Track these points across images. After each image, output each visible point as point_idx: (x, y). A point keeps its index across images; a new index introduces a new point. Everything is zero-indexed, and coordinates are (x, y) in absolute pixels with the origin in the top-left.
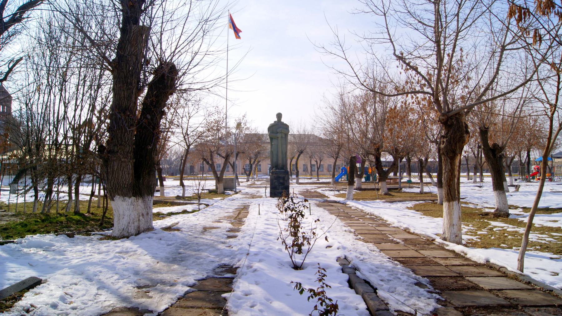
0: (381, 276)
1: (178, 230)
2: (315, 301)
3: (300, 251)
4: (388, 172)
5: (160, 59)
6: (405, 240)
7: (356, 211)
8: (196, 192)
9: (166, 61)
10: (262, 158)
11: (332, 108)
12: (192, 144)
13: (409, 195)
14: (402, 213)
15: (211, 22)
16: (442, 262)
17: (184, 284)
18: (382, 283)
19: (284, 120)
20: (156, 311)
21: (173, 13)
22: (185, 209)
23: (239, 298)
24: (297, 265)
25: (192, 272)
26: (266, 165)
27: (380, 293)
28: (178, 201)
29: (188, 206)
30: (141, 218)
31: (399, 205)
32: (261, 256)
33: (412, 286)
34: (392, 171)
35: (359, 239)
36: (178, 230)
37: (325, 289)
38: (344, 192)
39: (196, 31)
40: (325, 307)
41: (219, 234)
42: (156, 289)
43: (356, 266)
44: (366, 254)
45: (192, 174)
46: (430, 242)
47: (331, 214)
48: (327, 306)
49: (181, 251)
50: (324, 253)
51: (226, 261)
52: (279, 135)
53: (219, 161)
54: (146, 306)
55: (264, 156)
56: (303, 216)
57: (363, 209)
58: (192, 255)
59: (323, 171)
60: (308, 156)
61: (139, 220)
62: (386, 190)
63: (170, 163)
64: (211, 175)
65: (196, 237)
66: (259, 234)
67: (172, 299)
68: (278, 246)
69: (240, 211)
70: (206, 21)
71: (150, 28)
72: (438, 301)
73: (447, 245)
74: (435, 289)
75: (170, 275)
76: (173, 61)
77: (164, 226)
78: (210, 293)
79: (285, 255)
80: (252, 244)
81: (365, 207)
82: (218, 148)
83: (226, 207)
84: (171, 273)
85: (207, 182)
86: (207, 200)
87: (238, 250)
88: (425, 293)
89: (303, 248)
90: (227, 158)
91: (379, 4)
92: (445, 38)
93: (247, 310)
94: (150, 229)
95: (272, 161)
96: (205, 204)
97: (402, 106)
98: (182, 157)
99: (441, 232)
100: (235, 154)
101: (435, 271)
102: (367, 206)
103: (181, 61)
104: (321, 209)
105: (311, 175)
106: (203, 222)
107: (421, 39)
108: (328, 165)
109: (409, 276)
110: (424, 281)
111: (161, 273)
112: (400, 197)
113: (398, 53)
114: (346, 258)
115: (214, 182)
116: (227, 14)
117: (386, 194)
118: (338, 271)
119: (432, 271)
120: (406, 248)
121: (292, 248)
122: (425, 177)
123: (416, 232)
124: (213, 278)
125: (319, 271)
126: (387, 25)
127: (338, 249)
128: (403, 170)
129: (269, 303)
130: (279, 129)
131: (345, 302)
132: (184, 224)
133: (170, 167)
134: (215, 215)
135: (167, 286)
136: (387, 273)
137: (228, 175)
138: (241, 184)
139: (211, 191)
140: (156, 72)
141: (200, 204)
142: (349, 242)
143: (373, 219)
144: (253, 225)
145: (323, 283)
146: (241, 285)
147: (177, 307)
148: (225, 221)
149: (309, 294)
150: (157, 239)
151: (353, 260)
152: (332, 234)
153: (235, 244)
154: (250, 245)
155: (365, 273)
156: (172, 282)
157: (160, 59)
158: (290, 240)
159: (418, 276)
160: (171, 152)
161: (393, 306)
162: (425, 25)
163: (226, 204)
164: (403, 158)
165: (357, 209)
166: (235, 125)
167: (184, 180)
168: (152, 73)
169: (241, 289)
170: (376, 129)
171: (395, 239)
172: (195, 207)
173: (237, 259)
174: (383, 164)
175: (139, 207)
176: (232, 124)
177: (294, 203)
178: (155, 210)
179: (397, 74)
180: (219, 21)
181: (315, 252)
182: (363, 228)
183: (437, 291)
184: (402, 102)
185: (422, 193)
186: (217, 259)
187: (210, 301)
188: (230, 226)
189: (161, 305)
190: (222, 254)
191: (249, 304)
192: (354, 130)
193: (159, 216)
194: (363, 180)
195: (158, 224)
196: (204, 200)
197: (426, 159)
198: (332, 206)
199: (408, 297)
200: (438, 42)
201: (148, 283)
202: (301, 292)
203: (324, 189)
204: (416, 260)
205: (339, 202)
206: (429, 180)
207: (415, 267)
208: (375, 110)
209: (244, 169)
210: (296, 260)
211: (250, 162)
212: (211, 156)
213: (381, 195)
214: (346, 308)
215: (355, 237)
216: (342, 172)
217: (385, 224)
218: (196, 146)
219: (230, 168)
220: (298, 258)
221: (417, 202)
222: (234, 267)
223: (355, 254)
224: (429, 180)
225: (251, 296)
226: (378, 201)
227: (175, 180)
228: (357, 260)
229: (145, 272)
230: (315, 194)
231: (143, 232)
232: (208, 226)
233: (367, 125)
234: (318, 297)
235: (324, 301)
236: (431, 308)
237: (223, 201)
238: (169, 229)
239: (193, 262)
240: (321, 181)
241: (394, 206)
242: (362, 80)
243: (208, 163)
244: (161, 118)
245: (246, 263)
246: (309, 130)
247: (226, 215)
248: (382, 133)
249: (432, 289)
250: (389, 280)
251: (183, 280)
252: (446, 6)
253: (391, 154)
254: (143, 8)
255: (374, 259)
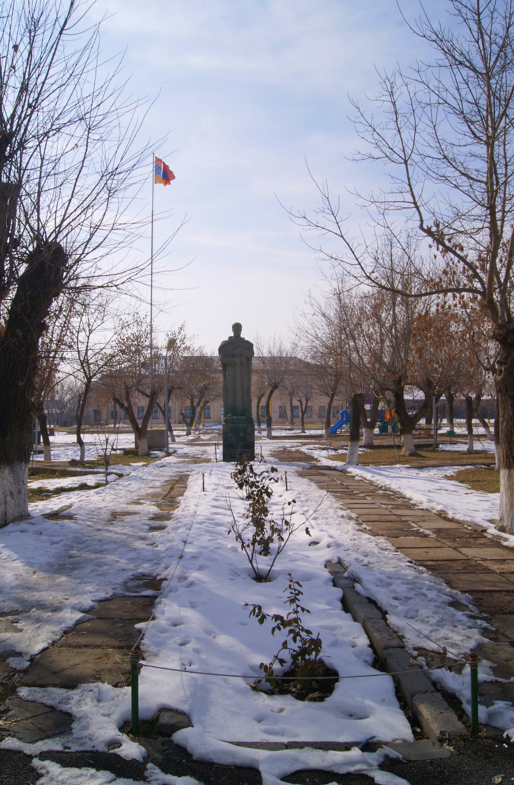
0: (395, 592)
1: (70, 517)
2: (283, 634)
3: (266, 551)
4: (417, 418)
5: (37, 237)
6: (438, 531)
7: (362, 483)
8: (102, 453)
9: (47, 240)
10: (212, 397)
11: (324, 315)
12: (95, 375)
13: (450, 456)
14: (437, 486)
15: (121, 176)
16: (495, 567)
17: (74, 608)
18: (396, 603)
19: (245, 335)
20: (27, 654)
21: (57, 161)
22: (85, 482)
23: (163, 631)
24: (261, 573)
25: (89, 588)
26: (217, 408)
27: (392, 619)
28: (74, 469)
29: (89, 477)
30: (9, 499)
31: (433, 472)
32: (202, 561)
33: (443, 608)
34: (423, 416)
35: (364, 531)
36: (70, 517)
37: (301, 615)
38: (344, 451)
39: (96, 191)
40: (300, 644)
41: (136, 524)
42: (29, 617)
43: (355, 575)
44: (373, 554)
45: (98, 424)
46: (477, 534)
47: (321, 488)
48: (304, 641)
49: (73, 552)
50: (306, 553)
51: (145, 568)
52: (237, 360)
53: (141, 402)
54: (11, 645)
55: (214, 393)
56: (269, 495)
57: (374, 479)
58: (91, 560)
59: (311, 417)
60: (287, 392)
61: (6, 502)
62: (412, 447)
63: (61, 404)
64: (128, 426)
65: (99, 530)
66: (202, 523)
67: (54, 632)
68: (231, 543)
69: (174, 485)
70: (112, 173)
71: (19, 185)
72: (484, 632)
73: (506, 540)
74: (481, 612)
75: (53, 593)
76: (58, 241)
77: (48, 512)
78: (117, 622)
79: (241, 558)
80: (189, 540)
81: (377, 477)
82: (139, 382)
83: (150, 478)
84: (55, 590)
85: (121, 436)
86: (120, 466)
87: (166, 550)
88: (465, 619)
89: (271, 545)
90: (153, 397)
91: (395, 144)
92: (504, 200)
93: (174, 650)
94: (25, 516)
95: (226, 402)
96: (116, 474)
97: (437, 310)
98: (80, 396)
99: (497, 517)
100: (165, 391)
101: (483, 582)
102: (380, 474)
103: (72, 240)
104: (305, 481)
105: (292, 423)
106: (111, 504)
107: (465, 204)
108: (320, 407)
109: (440, 591)
110: (464, 598)
111: (38, 590)
112: (435, 459)
113: (428, 223)
114: (340, 562)
115: (132, 437)
116: (150, 160)
117: (412, 455)
118: (326, 583)
119: (478, 582)
120: (439, 544)
121: (251, 546)
122: (477, 425)
123: (457, 517)
124: (123, 596)
125: (290, 586)
126: (409, 179)
127: (329, 546)
128: (441, 413)
129: (211, 638)
130: (236, 348)
131: (335, 635)
132: (80, 508)
133: (62, 413)
134: (132, 492)
135: (47, 612)
136: (405, 587)
137: (156, 426)
138: (177, 439)
139: (127, 452)
140: (31, 258)
141: (108, 474)
142: (346, 536)
143: (387, 497)
144: (192, 508)
145: (298, 606)
146: (167, 609)
147: (62, 646)
148: (148, 503)
149: (275, 624)
150: (35, 533)
151: (351, 564)
152: (320, 521)
153: (161, 540)
154: (185, 542)
155: (369, 586)
156: (56, 604)
157: (37, 237)
158: (249, 534)
159: (455, 591)
160: (63, 387)
161: (412, 640)
162: (472, 179)
163: (150, 474)
164: (441, 395)
165: (363, 480)
166: (165, 343)
167: (84, 433)
168: (24, 261)
169: (167, 615)
170: (395, 348)
171: (422, 530)
172: (101, 478)
173: (163, 565)
174: (407, 405)
175: (5, 481)
176: (161, 341)
177: (256, 475)
178: (35, 485)
179: (429, 259)
180: (134, 173)
181: (290, 553)
182: (372, 511)
183: (484, 615)
184: (438, 305)
185: (470, 452)
186: (131, 566)
187: (116, 636)
188: (154, 509)
189: (37, 643)
190: (139, 558)
191: (178, 640)
192: (361, 351)
193: (43, 494)
194: (376, 431)
195: (37, 507)
196: (115, 466)
197: (478, 397)
198: (324, 475)
199: (437, 625)
200: (492, 208)
201: (17, 606)
202: (261, 621)
203: (312, 446)
204: (454, 564)
205: (334, 469)
206: (481, 430)
207: (451, 577)
208: (394, 316)
209: (182, 414)
210: (260, 566)
211: (192, 402)
212: (128, 395)
213: (404, 456)
214: (335, 644)
215: (357, 527)
216: (342, 418)
217: (407, 504)
218: (103, 377)
219: (160, 414)
220: (262, 563)
221: (462, 468)
222: (158, 578)
223: (355, 555)
224: (481, 430)
225: (182, 626)
226: (398, 466)
227: (69, 433)
228: (359, 566)
229: (12, 588)
230: (297, 455)
231: (13, 521)
232: (119, 510)
233: (382, 341)
234: (288, 628)
235: (298, 634)
236: (472, 644)
237: (146, 469)
238: (55, 515)
239: (92, 571)
240: (308, 433)
241: (423, 474)
242: (368, 270)
243: (122, 406)
244: (40, 335)
245: (178, 572)
246: (287, 349)
247: (150, 491)
248: (406, 354)
249: (476, 611)
250: (407, 599)
251: (73, 601)
252: (507, 147)
253: (422, 389)
254: (7, 154)
255: (386, 564)
